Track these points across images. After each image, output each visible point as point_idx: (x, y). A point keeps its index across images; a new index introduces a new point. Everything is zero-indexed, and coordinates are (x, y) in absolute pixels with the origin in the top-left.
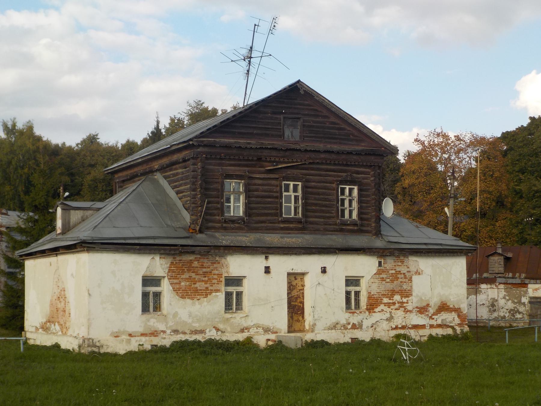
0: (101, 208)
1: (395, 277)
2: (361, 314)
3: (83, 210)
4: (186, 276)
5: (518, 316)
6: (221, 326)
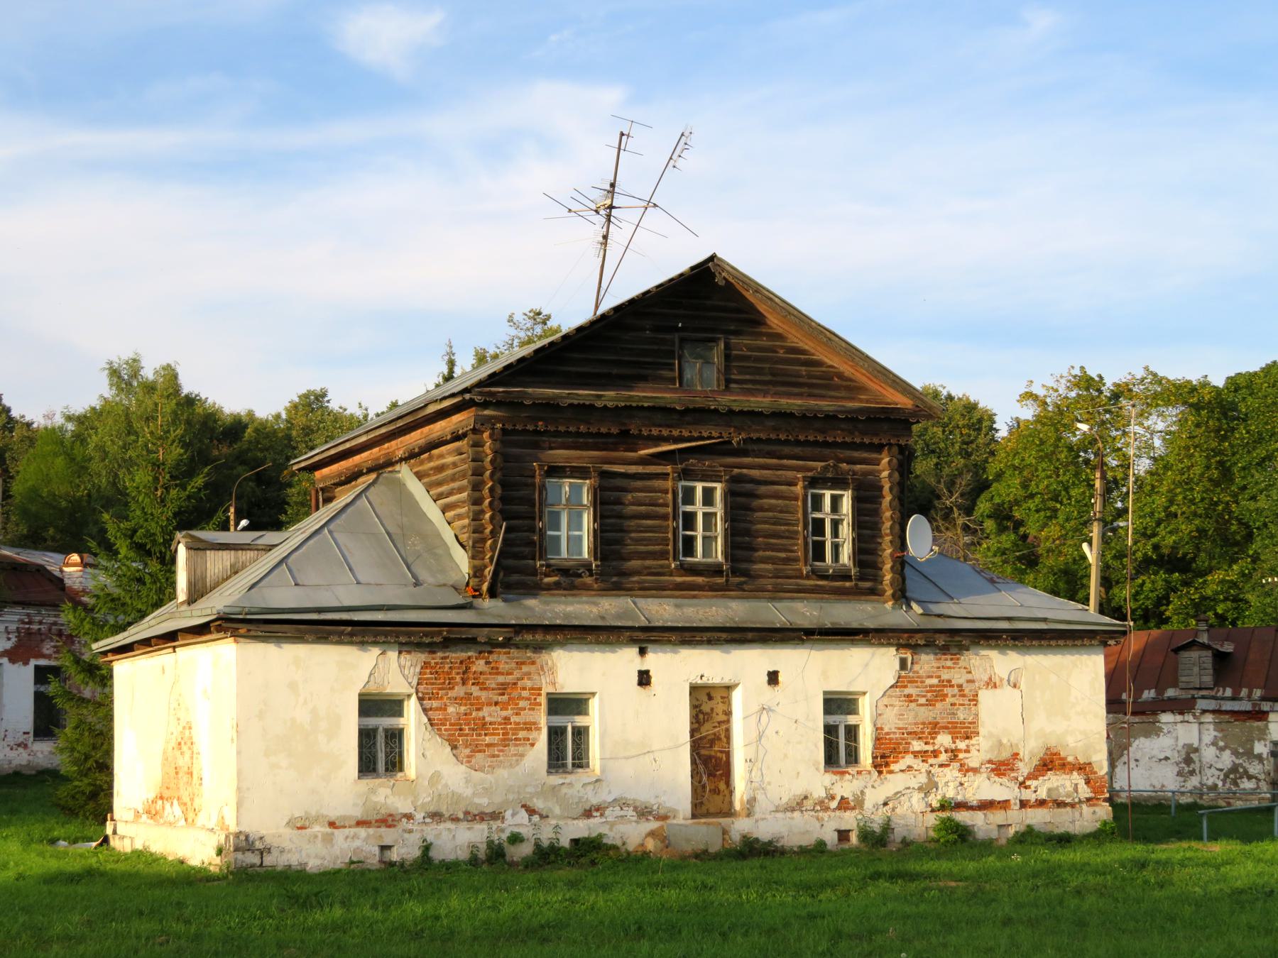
0: (277, 545)
1: (937, 695)
2: (860, 777)
3: (234, 549)
4: (459, 691)
5: (1247, 785)
6: (539, 804)
